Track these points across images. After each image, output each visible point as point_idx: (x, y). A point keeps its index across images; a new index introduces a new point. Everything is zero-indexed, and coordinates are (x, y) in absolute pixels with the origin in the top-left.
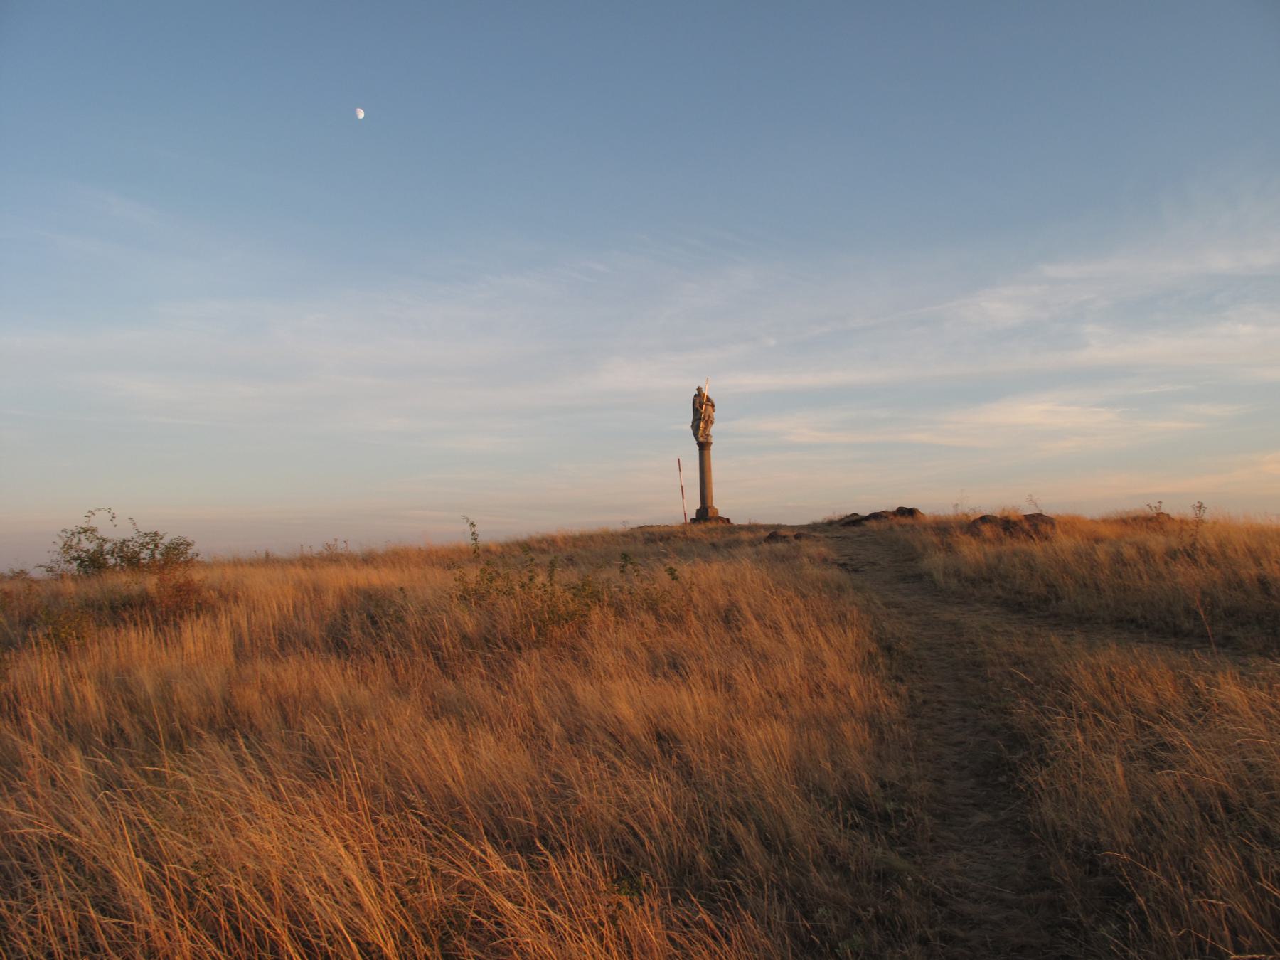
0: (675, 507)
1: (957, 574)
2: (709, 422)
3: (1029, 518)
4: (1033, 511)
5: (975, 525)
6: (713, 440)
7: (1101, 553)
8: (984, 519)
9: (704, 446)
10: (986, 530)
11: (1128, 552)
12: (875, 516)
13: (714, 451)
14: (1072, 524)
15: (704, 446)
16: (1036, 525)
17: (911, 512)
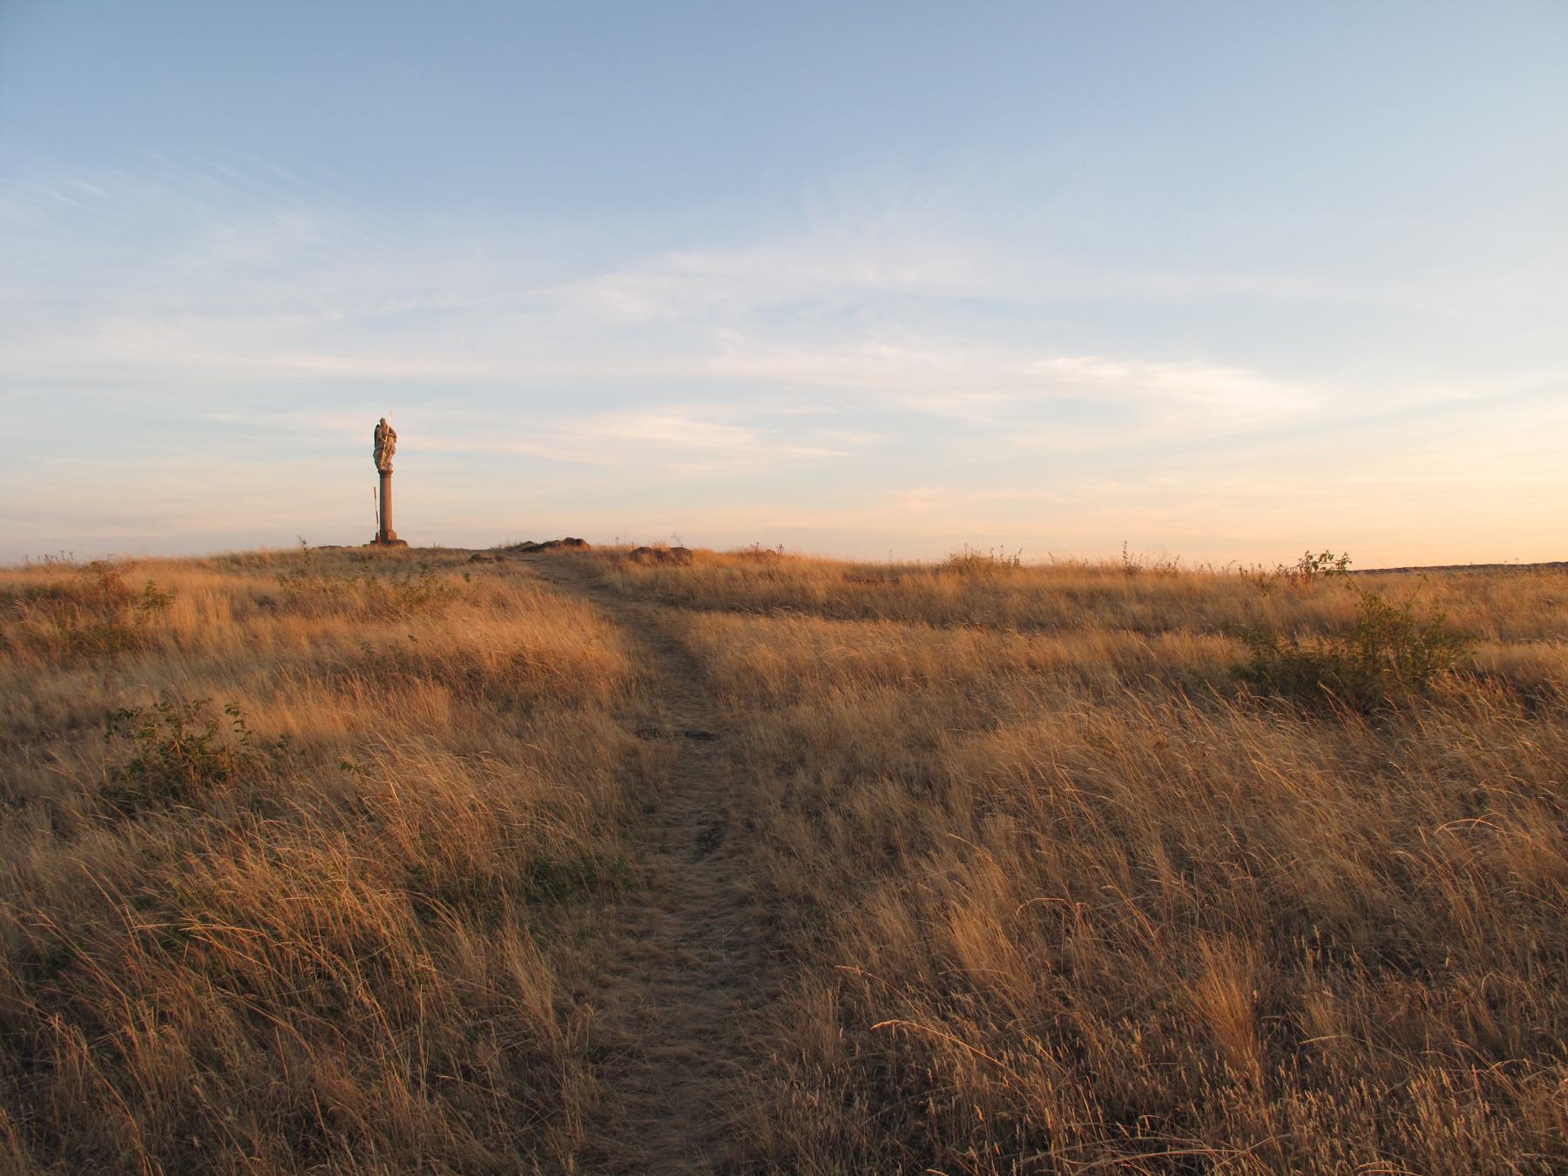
0: (359, 531)
1: (631, 584)
2: (391, 451)
3: (675, 550)
4: (675, 545)
5: (637, 554)
6: (393, 468)
7: (721, 573)
8: (642, 550)
9: (385, 474)
10: (646, 558)
11: (737, 573)
12: (549, 544)
13: (394, 479)
14: (705, 555)
15: (385, 474)
16: (680, 554)
17: (579, 542)
